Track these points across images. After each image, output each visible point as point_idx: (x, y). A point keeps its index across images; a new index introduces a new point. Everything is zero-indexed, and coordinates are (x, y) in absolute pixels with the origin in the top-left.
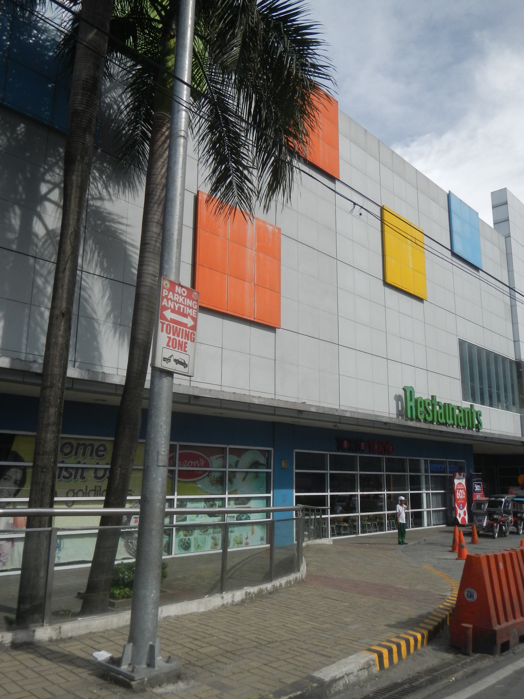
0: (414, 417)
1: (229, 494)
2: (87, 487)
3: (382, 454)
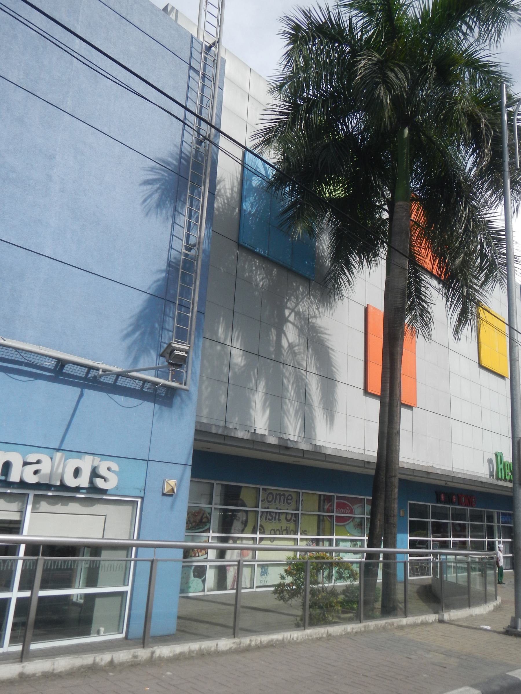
0: (503, 478)
1: (301, 534)
2: (281, 527)
3: (468, 506)
